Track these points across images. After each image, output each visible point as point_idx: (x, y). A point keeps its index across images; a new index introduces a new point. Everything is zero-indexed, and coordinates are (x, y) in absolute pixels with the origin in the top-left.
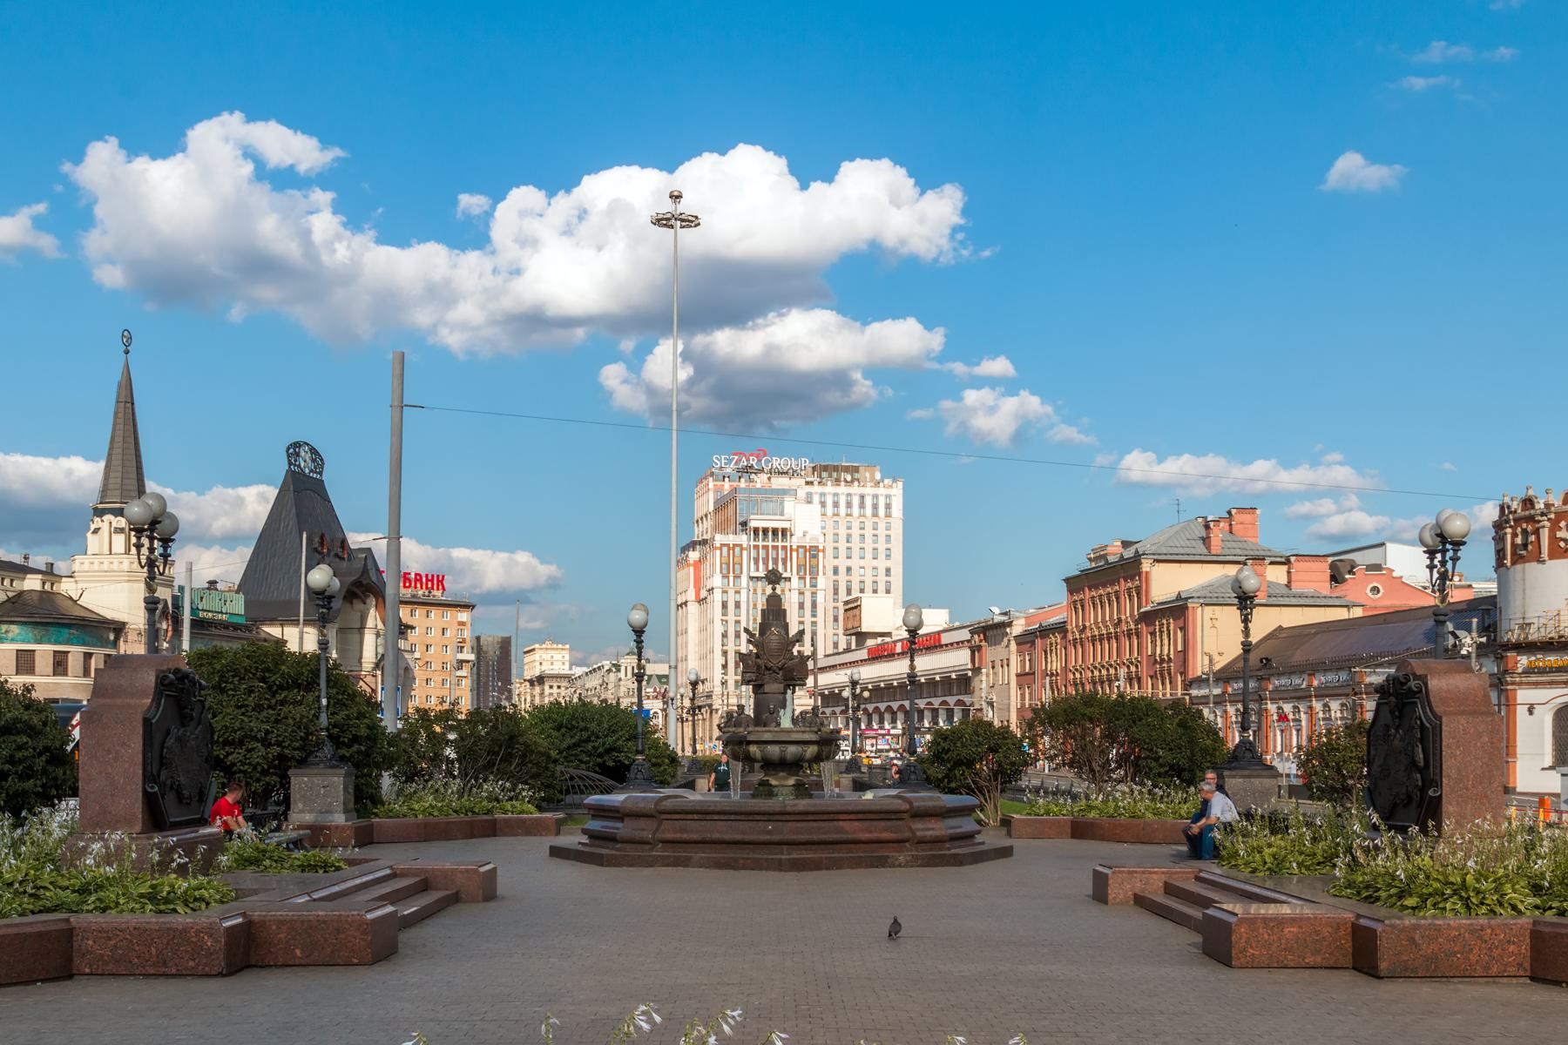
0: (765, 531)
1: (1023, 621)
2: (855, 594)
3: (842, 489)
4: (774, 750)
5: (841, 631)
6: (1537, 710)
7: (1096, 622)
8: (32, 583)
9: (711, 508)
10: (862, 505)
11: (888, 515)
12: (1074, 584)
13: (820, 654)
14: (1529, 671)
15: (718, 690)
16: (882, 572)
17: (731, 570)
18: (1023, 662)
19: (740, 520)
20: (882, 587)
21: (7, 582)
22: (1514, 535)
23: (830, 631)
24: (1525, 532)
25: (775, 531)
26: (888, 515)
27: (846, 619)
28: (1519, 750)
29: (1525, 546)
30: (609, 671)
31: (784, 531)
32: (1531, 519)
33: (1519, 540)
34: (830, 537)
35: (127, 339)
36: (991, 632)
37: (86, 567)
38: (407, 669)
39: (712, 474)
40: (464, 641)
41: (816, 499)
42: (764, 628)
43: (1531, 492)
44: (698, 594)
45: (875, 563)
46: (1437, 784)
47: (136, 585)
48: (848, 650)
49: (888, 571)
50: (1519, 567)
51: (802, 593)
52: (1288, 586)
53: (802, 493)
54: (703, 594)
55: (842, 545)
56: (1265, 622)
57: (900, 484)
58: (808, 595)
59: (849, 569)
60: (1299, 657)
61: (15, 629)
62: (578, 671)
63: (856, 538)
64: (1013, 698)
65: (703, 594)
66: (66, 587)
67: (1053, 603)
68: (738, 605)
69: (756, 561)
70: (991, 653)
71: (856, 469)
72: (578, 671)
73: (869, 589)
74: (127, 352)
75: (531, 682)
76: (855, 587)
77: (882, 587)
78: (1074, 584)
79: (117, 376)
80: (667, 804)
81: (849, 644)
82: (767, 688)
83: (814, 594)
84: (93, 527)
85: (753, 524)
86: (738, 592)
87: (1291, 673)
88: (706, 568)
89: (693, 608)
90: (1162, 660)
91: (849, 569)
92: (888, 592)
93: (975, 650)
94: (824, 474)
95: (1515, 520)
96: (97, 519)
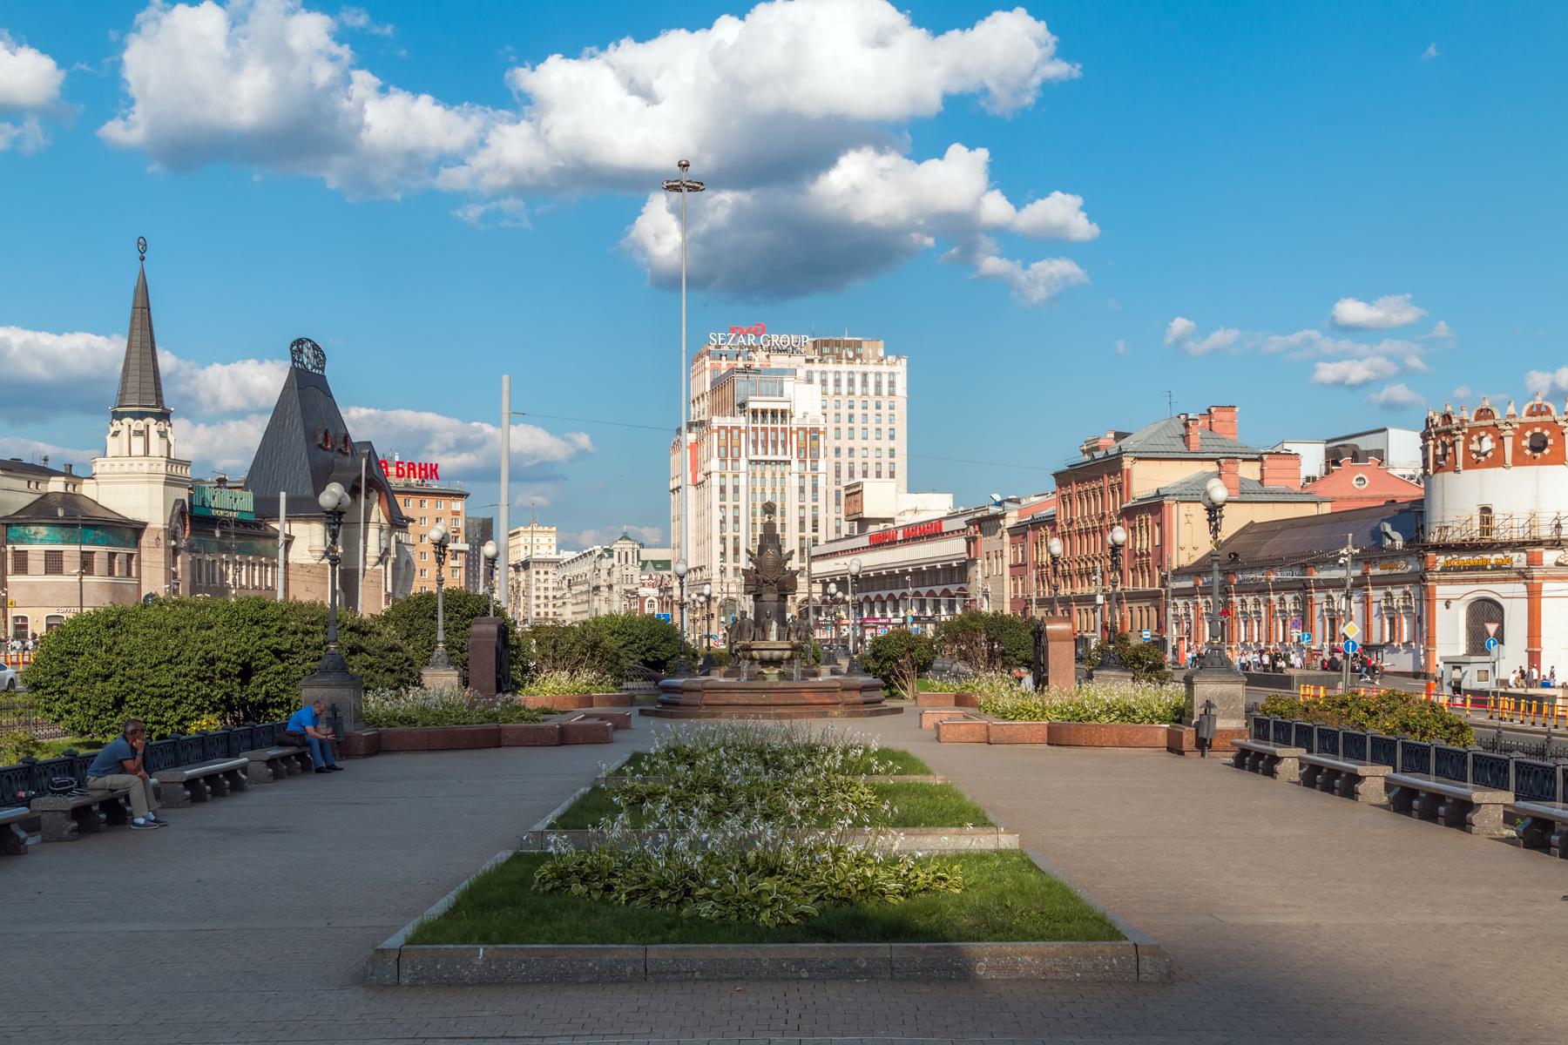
0: (764, 412)
1: (1016, 514)
2: (858, 478)
3: (844, 367)
4: (766, 654)
5: (843, 516)
6: (1453, 604)
7: (1083, 517)
8: (56, 485)
9: (708, 388)
10: (865, 383)
11: (892, 394)
12: (1063, 479)
13: (821, 541)
14: (1445, 570)
15: (716, 577)
16: (886, 453)
17: (729, 454)
18: (1016, 553)
19: (738, 400)
20: (885, 471)
21: (33, 485)
22: (1436, 447)
23: (832, 515)
24: (1443, 443)
25: (774, 413)
26: (892, 394)
27: (848, 505)
28: (1438, 640)
29: (1444, 456)
30: (601, 556)
31: (783, 413)
32: (1448, 433)
33: (1439, 452)
34: (831, 417)
35: (143, 246)
36: (987, 523)
37: (107, 469)
38: (409, 563)
39: (709, 353)
40: (458, 530)
41: (817, 378)
42: (762, 549)
43: (1449, 409)
44: (694, 477)
45: (878, 444)
46: (1046, 670)
47: (155, 486)
48: (848, 537)
49: (892, 453)
50: (1439, 475)
51: (802, 477)
52: (1261, 482)
53: (801, 373)
54: (700, 477)
55: (844, 425)
56: (1235, 520)
57: (904, 361)
58: (809, 479)
59: (851, 450)
60: (1263, 553)
61: (43, 531)
62: (567, 555)
63: (858, 418)
64: (1007, 590)
65: (700, 477)
66: (87, 489)
67: (1040, 500)
68: (736, 489)
69: (755, 443)
70: (986, 543)
71: (859, 344)
72: (567, 555)
73: (872, 472)
74: (142, 259)
75: (516, 568)
76: (858, 469)
77: (885, 471)
78: (1063, 479)
79: (133, 282)
80: (708, 685)
81: (852, 529)
82: (764, 597)
83: (815, 478)
84: (112, 430)
85: (752, 405)
86: (736, 476)
87: (1262, 568)
88: (703, 452)
89: (691, 491)
90: (1142, 554)
91: (851, 450)
92: (892, 475)
93: (971, 541)
94: (826, 350)
95: (1437, 433)
96: (116, 422)
